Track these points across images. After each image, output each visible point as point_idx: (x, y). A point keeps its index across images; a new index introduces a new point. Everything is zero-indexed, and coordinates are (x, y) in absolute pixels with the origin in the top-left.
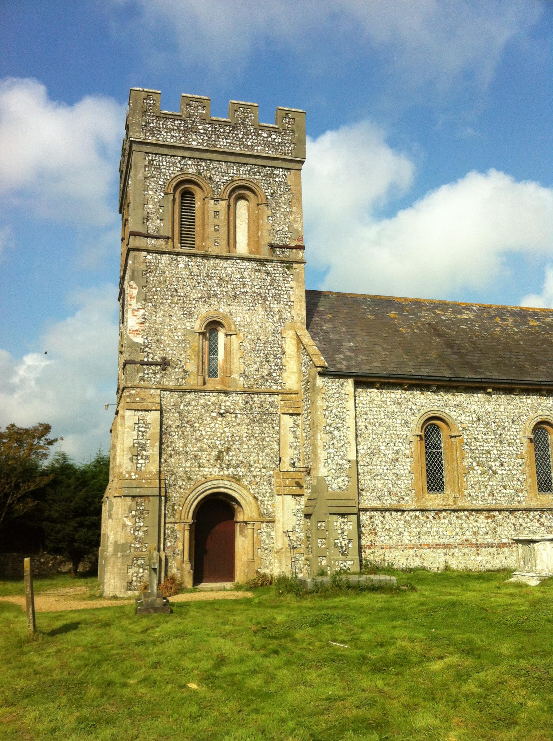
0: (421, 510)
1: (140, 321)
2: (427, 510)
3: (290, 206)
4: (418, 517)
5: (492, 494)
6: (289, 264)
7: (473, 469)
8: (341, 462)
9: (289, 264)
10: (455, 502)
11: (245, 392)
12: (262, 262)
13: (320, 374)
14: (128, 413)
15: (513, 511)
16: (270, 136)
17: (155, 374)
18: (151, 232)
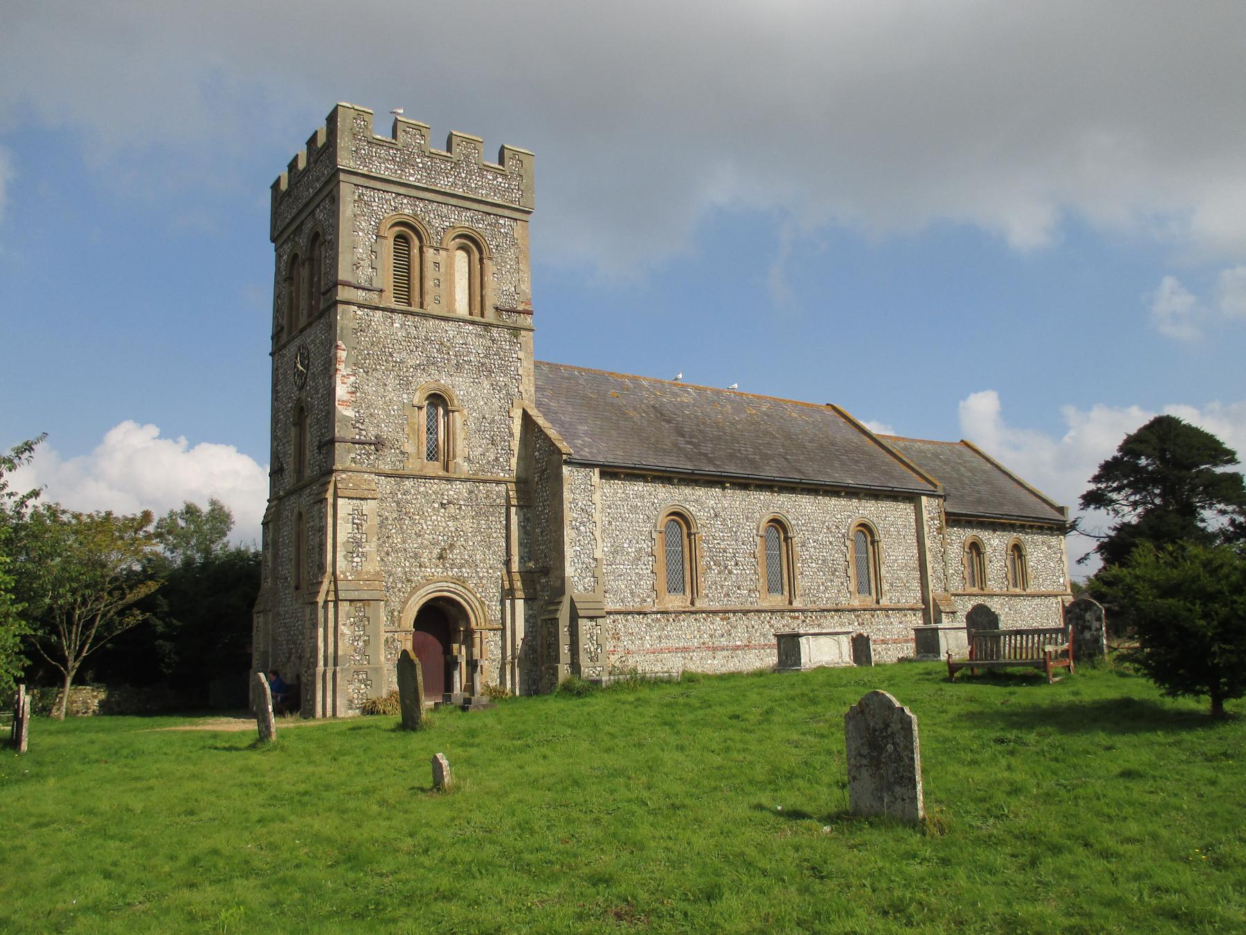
0: (662, 613)
2: (667, 613)
5: (727, 595)
6: (515, 330)
7: (710, 569)
9: (515, 330)
10: (692, 603)
15: (745, 612)
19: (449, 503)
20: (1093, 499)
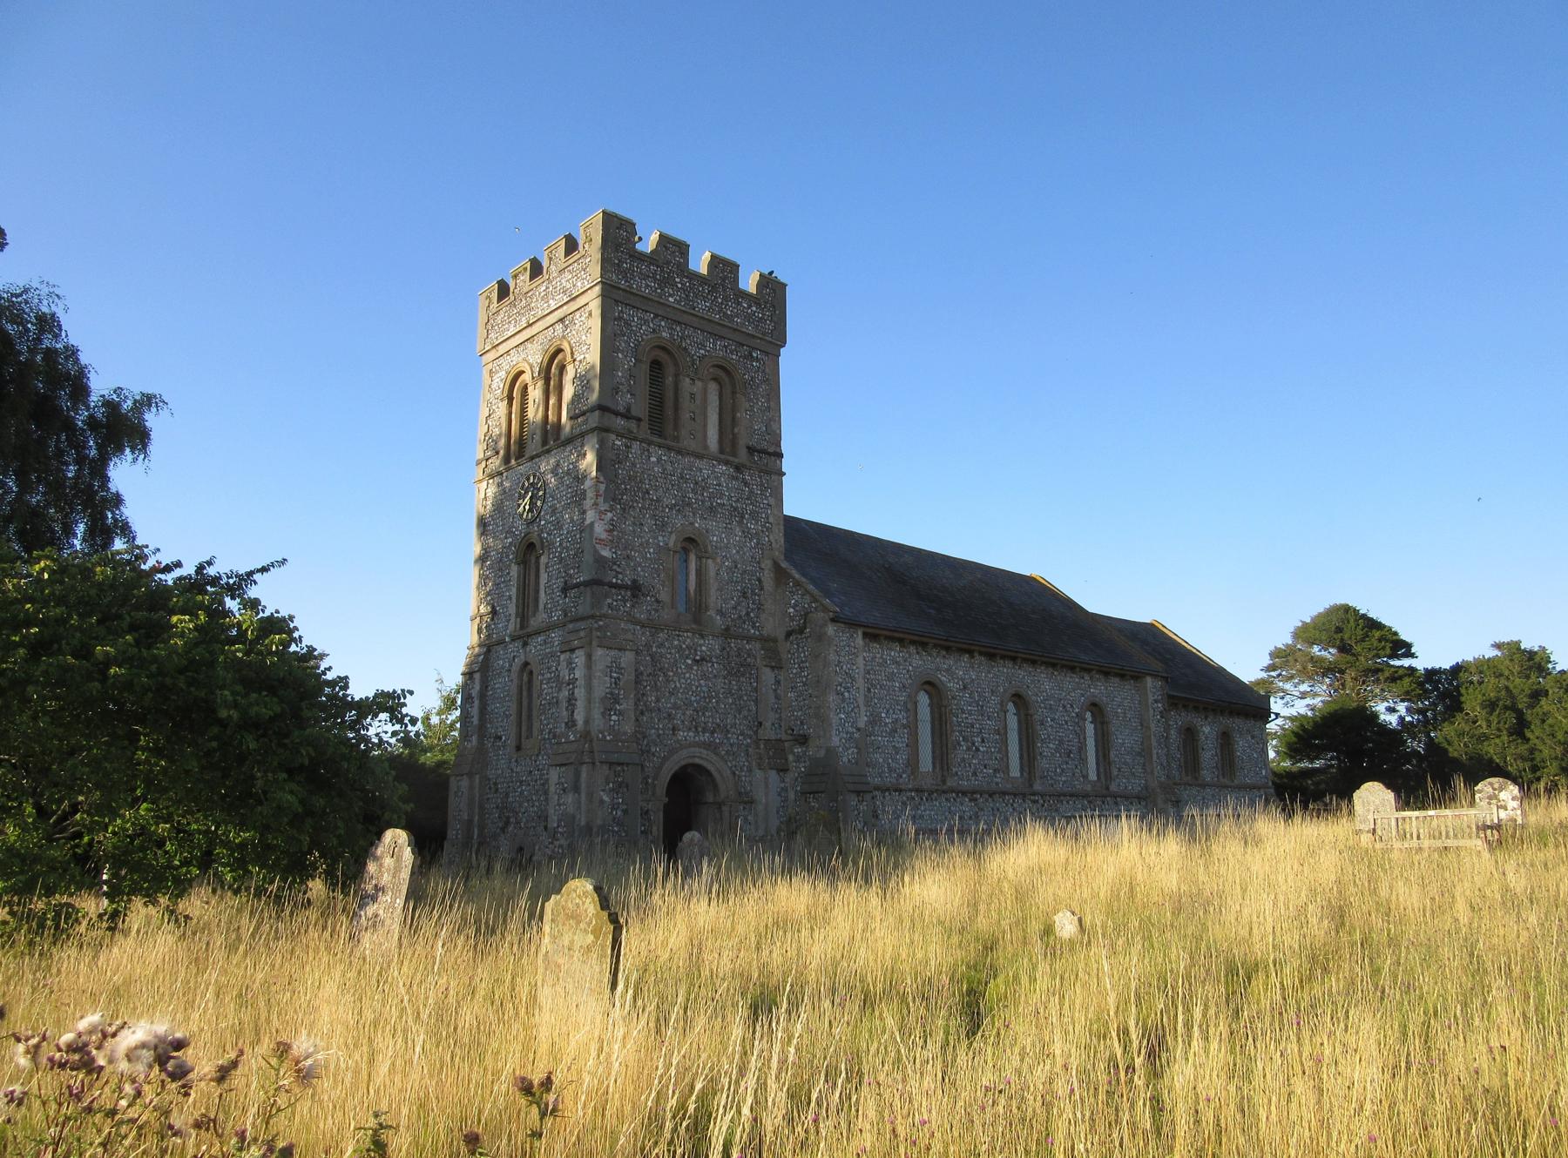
5: (975, 774)
13: (833, 620)
14: (600, 652)
18: (621, 409)
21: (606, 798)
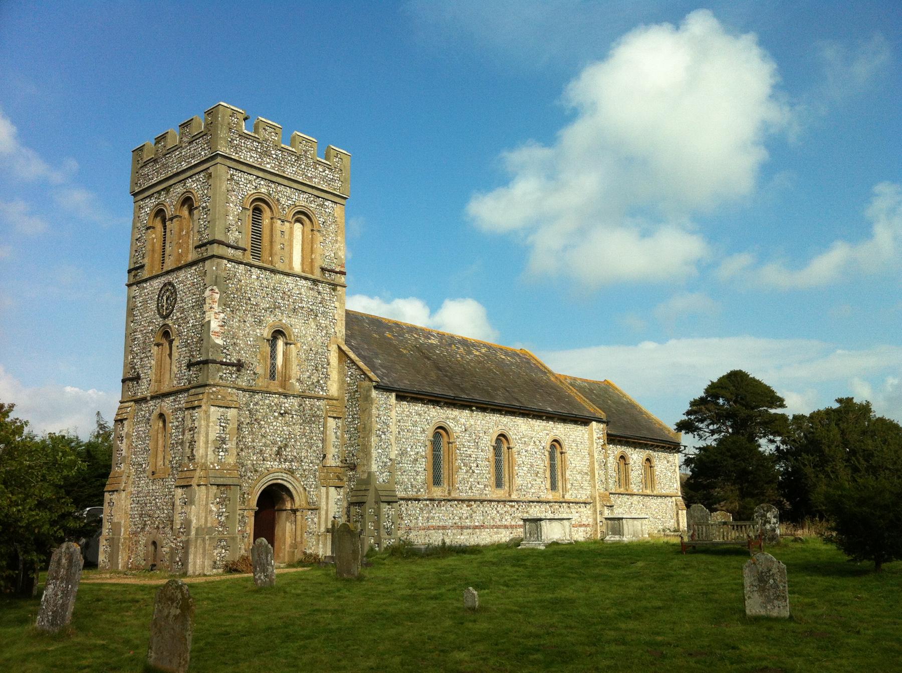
0: (430, 500)
1: (221, 323)
3: (336, 236)
4: (427, 505)
5: (471, 488)
6: (334, 286)
8: (385, 460)
9: (334, 286)
10: (449, 493)
11: (300, 396)
12: (315, 282)
13: (375, 387)
14: (213, 409)
15: (482, 501)
16: (324, 171)
17: (231, 374)
19: (286, 413)
20: (685, 426)
21: (214, 509)
